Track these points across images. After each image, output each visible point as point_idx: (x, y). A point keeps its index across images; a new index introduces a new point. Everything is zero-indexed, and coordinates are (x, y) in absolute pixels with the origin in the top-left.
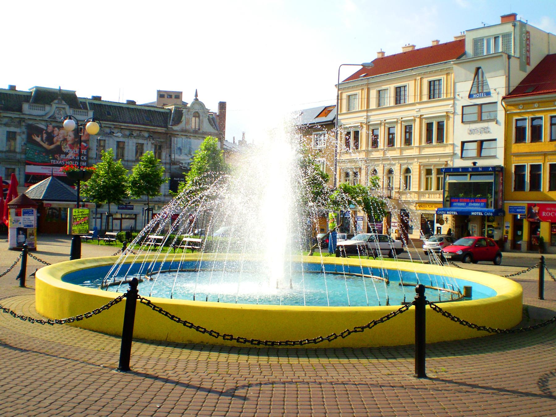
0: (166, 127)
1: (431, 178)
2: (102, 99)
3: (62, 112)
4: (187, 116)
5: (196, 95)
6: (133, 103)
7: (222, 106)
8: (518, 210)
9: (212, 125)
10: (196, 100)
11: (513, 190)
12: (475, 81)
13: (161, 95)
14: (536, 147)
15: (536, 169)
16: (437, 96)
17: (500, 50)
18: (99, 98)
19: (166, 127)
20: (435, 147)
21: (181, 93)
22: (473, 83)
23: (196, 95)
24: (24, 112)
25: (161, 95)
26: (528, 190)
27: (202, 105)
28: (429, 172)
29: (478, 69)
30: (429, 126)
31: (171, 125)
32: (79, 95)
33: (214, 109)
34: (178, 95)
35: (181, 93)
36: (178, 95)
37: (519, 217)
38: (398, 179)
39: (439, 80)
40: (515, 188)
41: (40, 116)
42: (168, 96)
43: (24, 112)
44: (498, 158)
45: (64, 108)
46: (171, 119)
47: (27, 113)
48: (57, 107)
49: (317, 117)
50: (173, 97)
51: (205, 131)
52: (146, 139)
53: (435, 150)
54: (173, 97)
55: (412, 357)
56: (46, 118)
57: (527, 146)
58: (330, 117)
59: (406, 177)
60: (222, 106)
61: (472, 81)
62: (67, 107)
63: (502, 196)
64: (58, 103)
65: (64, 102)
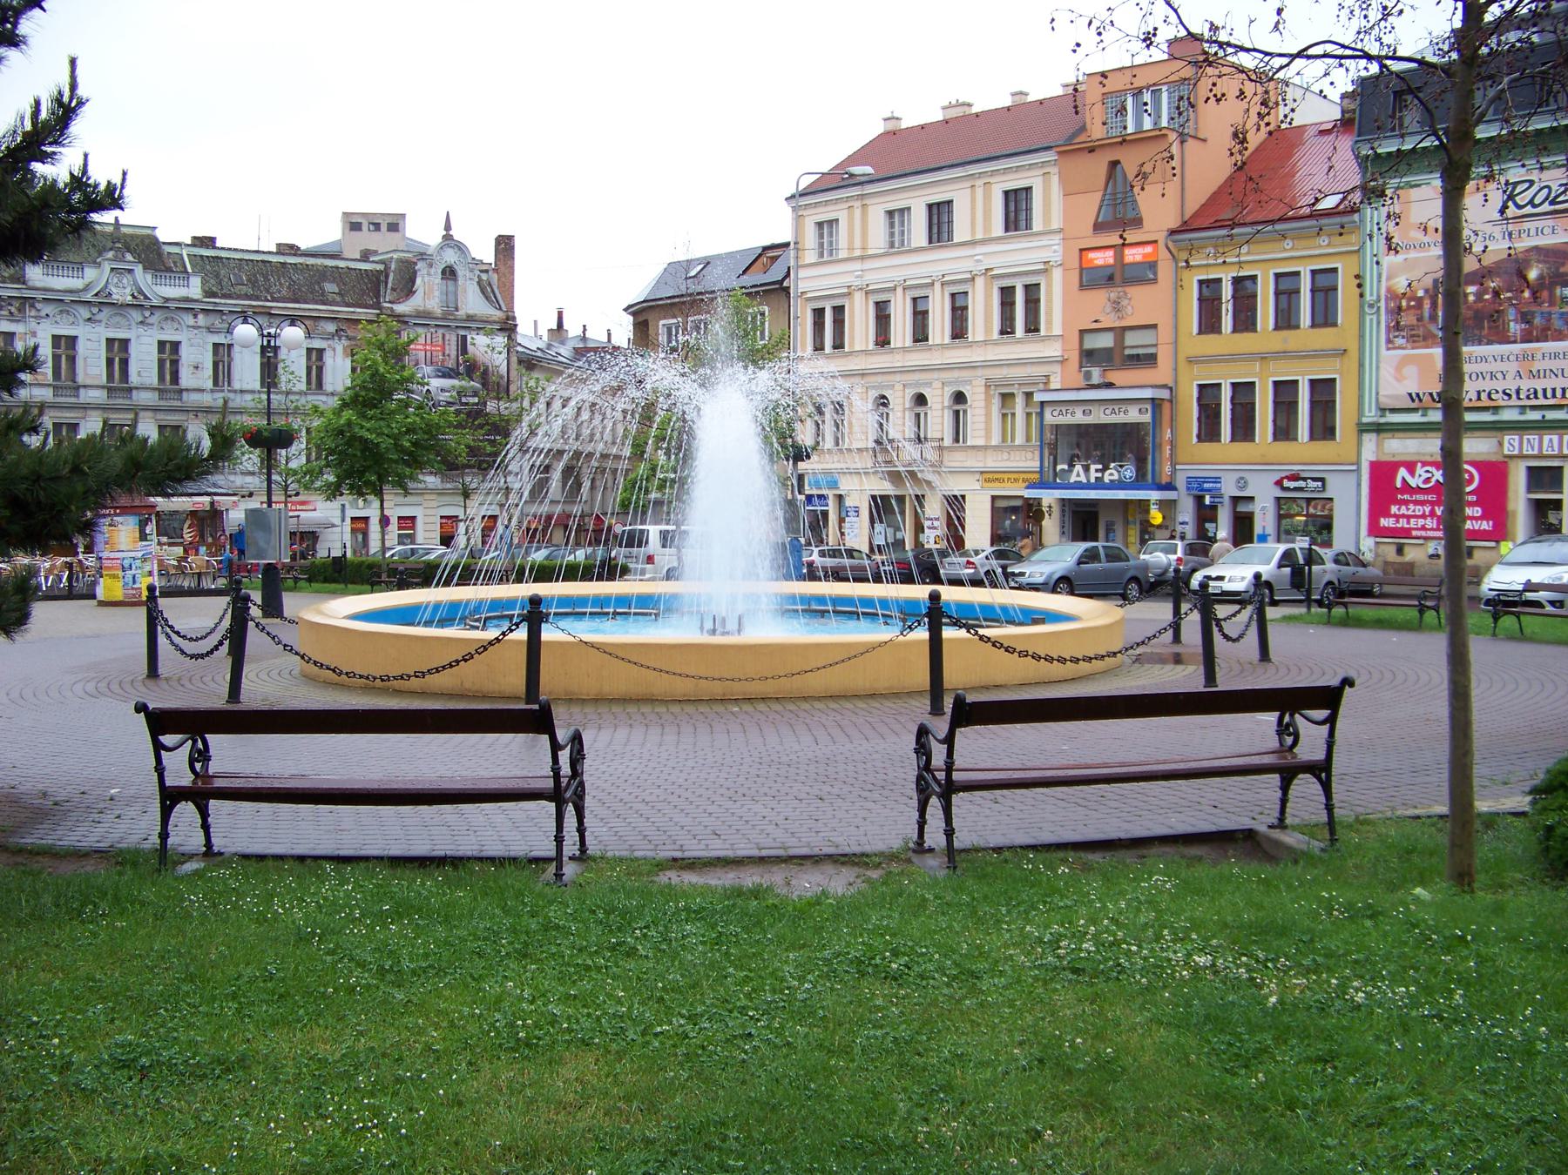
0: (377, 305)
1: (1013, 415)
2: (218, 244)
3: (125, 281)
4: (426, 279)
5: (448, 227)
6: (292, 249)
7: (505, 245)
8: (1206, 486)
9: (487, 298)
10: (448, 237)
11: (1195, 440)
12: (1109, 191)
13: (353, 224)
14: (1245, 342)
15: (1243, 391)
16: (1023, 224)
17: (1164, 123)
18: (209, 242)
19: (377, 305)
20: (1020, 341)
21: (403, 216)
22: (1104, 195)
23: (448, 227)
24: (30, 284)
25: (353, 224)
26: (1228, 439)
27: (460, 248)
28: (1007, 398)
29: (1114, 164)
30: (1007, 294)
31: (390, 302)
32: (163, 236)
33: (485, 252)
34: (395, 224)
35: (403, 216)
36: (395, 224)
37: (1207, 500)
38: (938, 421)
39: (1028, 190)
40: (1199, 436)
41: (71, 292)
42: (372, 227)
43: (30, 284)
44: (1348, 682)
45: (130, 271)
46: (390, 285)
47: (38, 284)
48: (112, 269)
49: (744, 272)
50: (384, 227)
51: (471, 312)
52: (331, 336)
53: (1021, 348)
54: (384, 227)
55: (1479, 815)
56: (89, 297)
57: (1227, 339)
58: (775, 274)
59: (957, 413)
60: (505, 245)
61: (1100, 194)
62: (139, 269)
63: (1171, 455)
64: (115, 260)
65: (129, 257)
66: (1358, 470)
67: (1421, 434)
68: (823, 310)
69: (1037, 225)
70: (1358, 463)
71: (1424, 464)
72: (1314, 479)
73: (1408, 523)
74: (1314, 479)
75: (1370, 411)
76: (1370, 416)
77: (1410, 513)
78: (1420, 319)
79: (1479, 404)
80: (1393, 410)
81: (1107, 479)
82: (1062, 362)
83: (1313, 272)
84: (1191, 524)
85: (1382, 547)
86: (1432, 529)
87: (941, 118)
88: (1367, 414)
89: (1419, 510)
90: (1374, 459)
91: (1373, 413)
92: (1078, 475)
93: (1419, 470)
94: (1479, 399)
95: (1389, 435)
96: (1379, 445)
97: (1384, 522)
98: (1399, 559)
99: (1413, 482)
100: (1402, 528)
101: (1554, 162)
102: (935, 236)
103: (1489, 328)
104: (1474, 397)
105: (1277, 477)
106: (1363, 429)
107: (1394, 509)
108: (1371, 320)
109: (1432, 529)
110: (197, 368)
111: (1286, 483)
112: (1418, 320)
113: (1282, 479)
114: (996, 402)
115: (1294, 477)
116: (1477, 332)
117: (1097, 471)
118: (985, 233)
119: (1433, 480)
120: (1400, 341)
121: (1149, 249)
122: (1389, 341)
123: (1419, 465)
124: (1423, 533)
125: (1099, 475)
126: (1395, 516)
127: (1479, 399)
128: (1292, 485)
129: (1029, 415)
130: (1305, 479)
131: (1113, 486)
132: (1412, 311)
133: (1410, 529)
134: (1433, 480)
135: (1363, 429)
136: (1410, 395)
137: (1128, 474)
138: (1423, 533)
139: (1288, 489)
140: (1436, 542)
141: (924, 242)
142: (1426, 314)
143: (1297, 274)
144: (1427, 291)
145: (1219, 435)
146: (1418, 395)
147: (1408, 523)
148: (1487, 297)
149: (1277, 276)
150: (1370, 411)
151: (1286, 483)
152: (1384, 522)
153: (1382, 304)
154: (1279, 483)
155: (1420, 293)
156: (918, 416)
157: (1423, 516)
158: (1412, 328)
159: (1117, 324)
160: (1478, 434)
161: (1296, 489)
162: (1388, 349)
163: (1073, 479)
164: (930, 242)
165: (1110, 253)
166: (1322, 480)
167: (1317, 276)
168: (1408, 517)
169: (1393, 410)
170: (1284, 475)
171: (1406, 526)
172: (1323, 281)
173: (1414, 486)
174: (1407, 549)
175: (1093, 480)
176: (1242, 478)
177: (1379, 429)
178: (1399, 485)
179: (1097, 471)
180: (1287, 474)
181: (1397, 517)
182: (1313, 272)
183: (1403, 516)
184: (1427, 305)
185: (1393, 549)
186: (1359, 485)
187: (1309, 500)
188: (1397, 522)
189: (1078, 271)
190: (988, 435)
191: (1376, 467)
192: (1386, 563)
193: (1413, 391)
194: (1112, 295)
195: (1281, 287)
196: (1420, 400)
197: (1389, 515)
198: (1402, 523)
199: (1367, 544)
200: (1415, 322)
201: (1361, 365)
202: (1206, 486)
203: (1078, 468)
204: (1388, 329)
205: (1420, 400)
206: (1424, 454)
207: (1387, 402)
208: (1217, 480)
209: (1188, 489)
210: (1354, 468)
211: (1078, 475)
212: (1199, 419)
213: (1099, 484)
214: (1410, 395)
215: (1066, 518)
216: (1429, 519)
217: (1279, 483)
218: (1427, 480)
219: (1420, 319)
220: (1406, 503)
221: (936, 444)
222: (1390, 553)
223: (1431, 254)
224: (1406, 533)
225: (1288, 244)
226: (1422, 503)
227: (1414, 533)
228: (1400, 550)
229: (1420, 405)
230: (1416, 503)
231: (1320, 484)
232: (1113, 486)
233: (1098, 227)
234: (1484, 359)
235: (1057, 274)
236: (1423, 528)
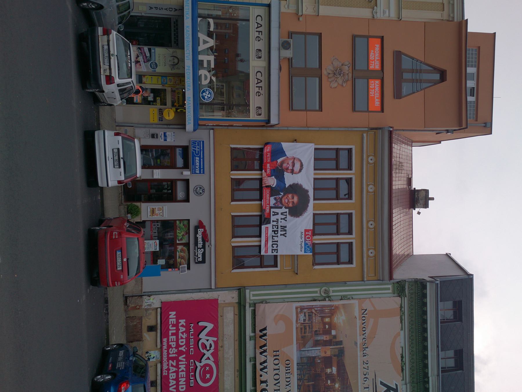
8: (197, 158)
66: (210, 289)
67: (237, 337)
70: (217, 289)
71: (216, 343)
72: (204, 255)
73: (173, 334)
74: (204, 255)
75: (254, 295)
76: (250, 296)
77: (180, 335)
78: (316, 333)
79: (258, 382)
80: (254, 313)
81: (203, 72)
82: (297, 14)
83: (350, 244)
85: (153, 313)
86: (168, 354)
88: (252, 293)
89: (182, 342)
90: (219, 302)
91: (252, 298)
92: (205, 42)
93: (211, 339)
94: (262, 382)
95: (237, 312)
96: (229, 304)
97: (173, 314)
98: (145, 329)
99: (203, 335)
100: (168, 330)
101: (405, 364)
103: (309, 386)
104: (263, 379)
105: (205, 223)
106: (241, 291)
107: (182, 322)
108: (316, 292)
109: (168, 354)
110: (400, 343)
111: (200, 231)
112: (316, 331)
113: (204, 227)
115: (205, 238)
116: (306, 378)
117: (209, 62)
119: (204, 351)
120: (302, 317)
121: (377, 103)
122: (302, 308)
123: (215, 339)
124: (165, 347)
125: (205, 65)
126: (178, 322)
127: (262, 382)
128: (200, 236)
130: (204, 247)
131: (196, 79)
132: (322, 327)
133: (168, 337)
134: (204, 351)
135: (241, 291)
136: (265, 329)
137: (206, 95)
138: (165, 347)
139: (196, 233)
140: (159, 356)
142: (319, 338)
144: (335, 337)
146: (265, 335)
147: (173, 334)
148: (329, 382)
149: (350, 151)
150: (254, 295)
151: (200, 231)
152: (173, 314)
153: (327, 303)
154: (200, 225)
155: (333, 332)
157: (178, 346)
158: (311, 327)
159: (324, 72)
160: (237, 380)
161: (196, 239)
162: (297, 308)
163: (202, 37)
165: (378, 67)
166: (203, 261)
168: (176, 334)
169: (254, 313)
170: (207, 228)
171: (170, 332)
172: (343, 188)
173: (200, 336)
174: (153, 333)
175: (201, 57)
176: (203, 191)
177: (241, 305)
178: (201, 324)
179: (209, 62)
180: (208, 232)
181: (176, 325)
182: (350, 244)
183: (178, 330)
184: (325, 338)
185: (152, 323)
186: (200, 290)
187: (187, 245)
188: (173, 325)
189: (367, 34)
191: (214, 302)
192: (141, 318)
193: (268, 332)
194: (346, 68)
195: (341, 153)
196: (261, 337)
197: (178, 318)
198: (172, 330)
199: (155, 302)
200: (314, 329)
201: (286, 286)
203: (212, 43)
204: (310, 308)
205: (261, 337)
206: (223, 340)
207: (260, 308)
208: (202, 171)
209: (194, 142)
210: (213, 287)
211: (205, 42)
213: (197, 64)
214: (265, 329)
215: (168, 12)
216: (175, 350)
217: (200, 225)
218: (204, 346)
219: (316, 333)
220: (187, 331)
222: (149, 321)
223: (358, 337)
224: (165, 334)
225: (371, 188)
226: (187, 344)
227: (165, 340)
228: (151, 329)
229: (258, 336)
230: (188, 339)
231: (200, 259)
232: (196, 79)
233: (398, 55)
234: (288, 384)
235: (365, 13)
236: (169, 346)
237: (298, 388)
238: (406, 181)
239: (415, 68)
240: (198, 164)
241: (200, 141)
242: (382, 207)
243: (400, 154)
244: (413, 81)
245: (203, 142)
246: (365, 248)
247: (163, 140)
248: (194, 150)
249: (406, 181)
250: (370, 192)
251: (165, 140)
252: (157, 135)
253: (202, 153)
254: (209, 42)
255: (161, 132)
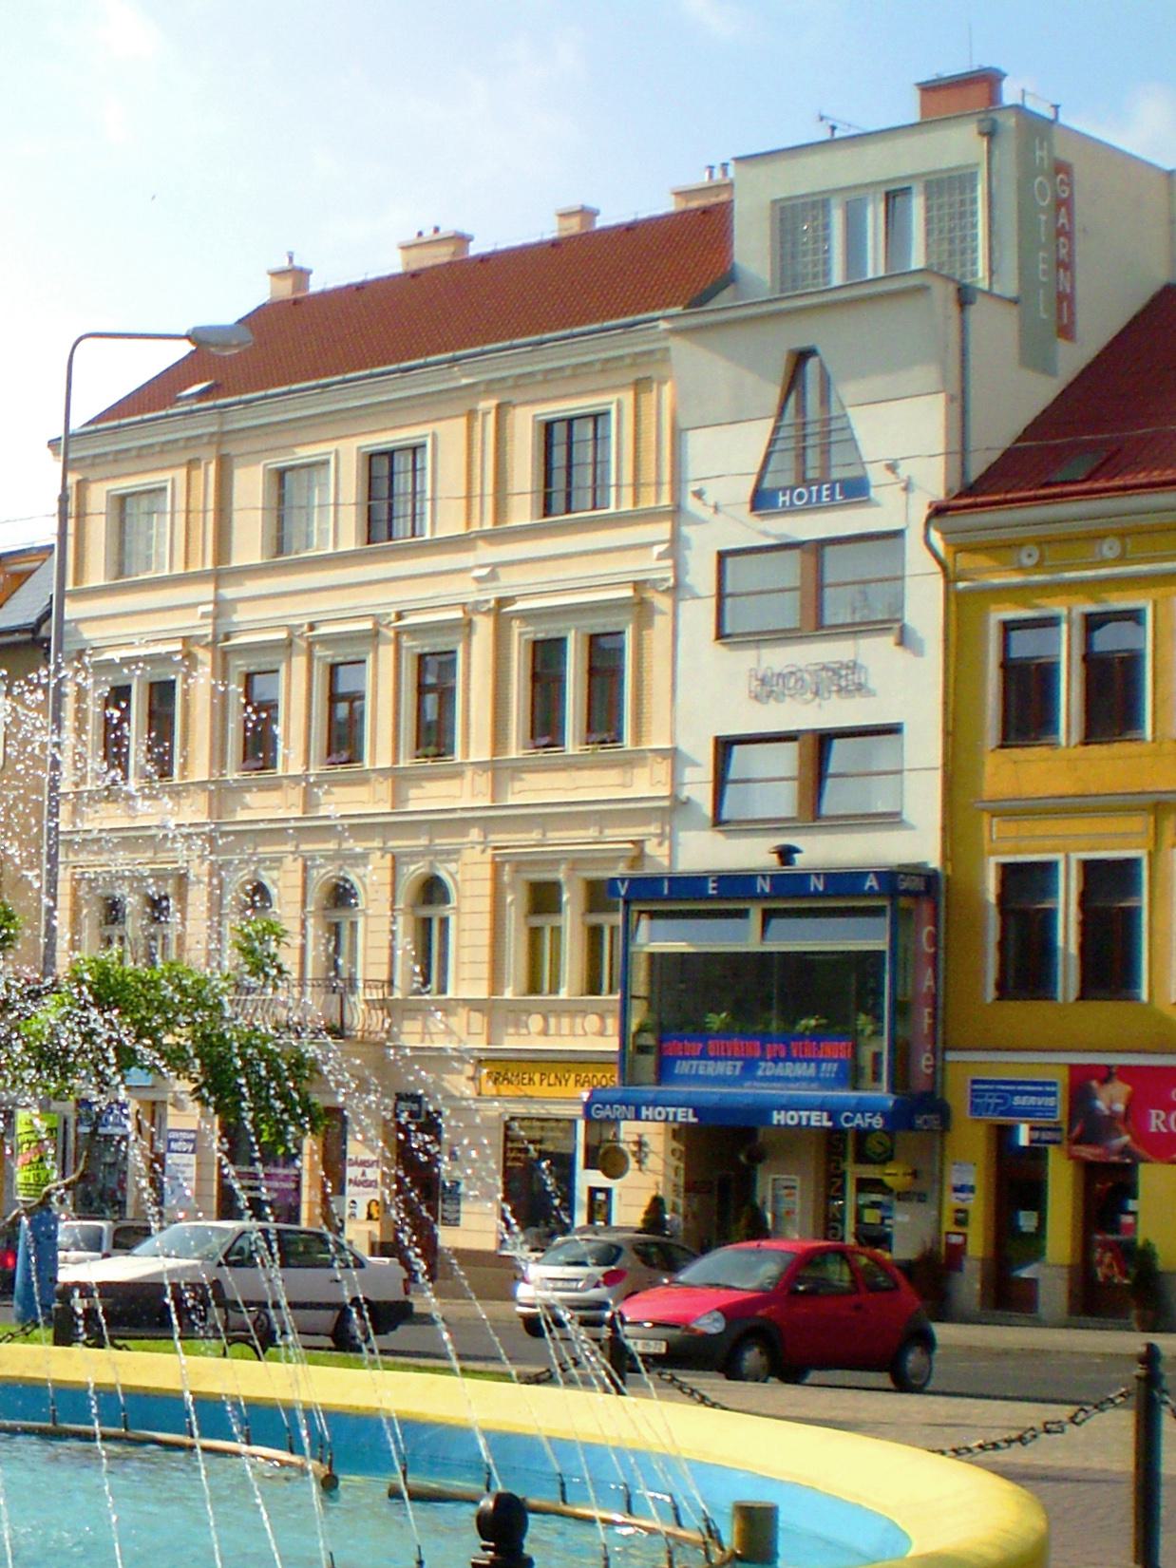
1: (557, 931)
8: (1017, 1101)
11: (991, 993)
17: (917, 260)
20: (574, 764)
22: (776, 430)
26: (1073, 991)
28: (543, 898)
30: (546, 656)
37: (1024, 1137)
40: (1001, 987)
61: (770, 423)
63: (933, 1027)
68: (559, 643)
69: (618, 501)
84: (980, 1192)
87: (398, 269)
102: (558, 501)
114: (515, 902)
118: (496, 522)
129: (595, 933)
141: (350, 540)
143: (1051, 622)
145: (1055, 991)
156: (426, 924)
164: (547, 511)
167: (1014, 634)
190: (496, 980)
202: (1017, 1101)
209: (975, 1108)
212: (1002, 945)
221: (376, 995)
237: (830, 270)
238: (356, 504)
239: (832, 439)
240: (1033, 1100)
241: (973, 1091)
242: (1068, 700)
243: (965, 297)
244: (825, 451)
245: (974, 1082)
246: (398, 437)
247: (971, 1196)
248: (994, 1111)
249: (356, 504)
250: (1042, 557)
251: (971, 1189)
252: (958, 1211)
253: (1003, 1087)
254: (912, 828)
255: (952, 1200)
